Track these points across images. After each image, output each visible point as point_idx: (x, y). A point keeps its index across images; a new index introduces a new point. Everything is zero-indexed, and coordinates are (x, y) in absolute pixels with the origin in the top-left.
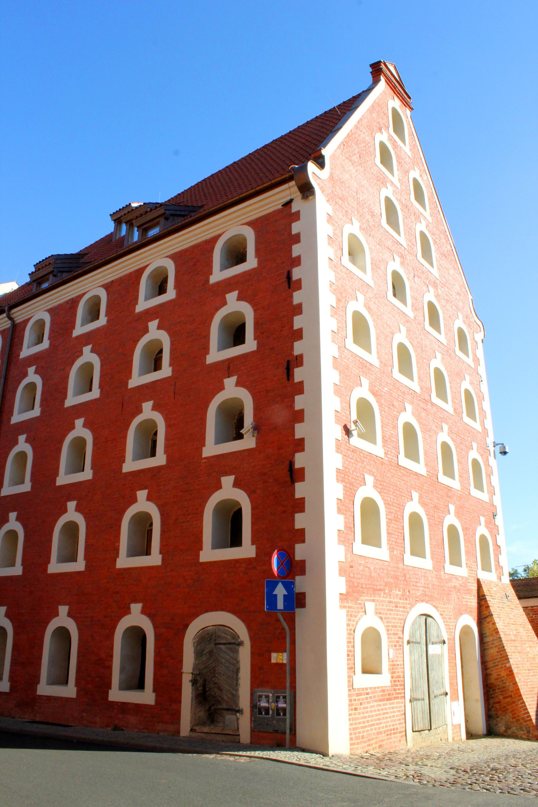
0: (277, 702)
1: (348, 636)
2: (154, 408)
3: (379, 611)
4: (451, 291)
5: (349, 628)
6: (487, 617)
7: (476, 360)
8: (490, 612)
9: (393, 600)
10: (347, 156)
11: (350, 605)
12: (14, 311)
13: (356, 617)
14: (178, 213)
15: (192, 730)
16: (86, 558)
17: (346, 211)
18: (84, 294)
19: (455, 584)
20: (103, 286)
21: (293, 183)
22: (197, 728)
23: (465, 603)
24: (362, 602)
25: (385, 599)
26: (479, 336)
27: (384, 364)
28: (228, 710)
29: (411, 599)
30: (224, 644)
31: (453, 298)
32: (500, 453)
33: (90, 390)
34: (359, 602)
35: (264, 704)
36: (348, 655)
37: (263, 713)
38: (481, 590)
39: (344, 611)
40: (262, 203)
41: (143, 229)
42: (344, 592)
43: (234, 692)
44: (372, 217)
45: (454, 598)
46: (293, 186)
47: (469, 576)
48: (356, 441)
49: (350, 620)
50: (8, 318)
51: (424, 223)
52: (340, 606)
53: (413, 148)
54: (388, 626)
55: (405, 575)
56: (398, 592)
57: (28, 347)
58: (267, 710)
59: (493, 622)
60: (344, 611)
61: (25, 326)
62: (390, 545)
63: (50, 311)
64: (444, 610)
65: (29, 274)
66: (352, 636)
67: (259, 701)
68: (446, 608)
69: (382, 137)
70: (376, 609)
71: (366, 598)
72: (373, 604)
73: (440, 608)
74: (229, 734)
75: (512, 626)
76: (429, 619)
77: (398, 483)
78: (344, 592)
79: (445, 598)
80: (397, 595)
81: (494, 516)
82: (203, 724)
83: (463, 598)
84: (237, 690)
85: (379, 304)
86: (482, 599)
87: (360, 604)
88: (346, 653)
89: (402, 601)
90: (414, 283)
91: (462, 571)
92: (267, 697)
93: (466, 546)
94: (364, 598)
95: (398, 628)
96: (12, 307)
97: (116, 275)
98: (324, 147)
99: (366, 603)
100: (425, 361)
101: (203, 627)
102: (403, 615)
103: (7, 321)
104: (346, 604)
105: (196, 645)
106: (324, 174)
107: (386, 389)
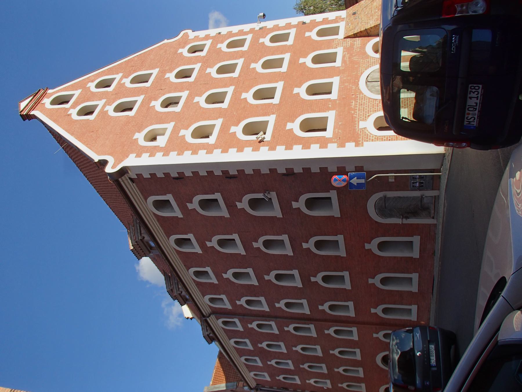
0: (416, 178)
1: (379, 140)
2: (256, 241)
3: (364, 118)
4: (165, 58)
5: (374, 140)
6: (367, 32)
7: (207, 37)
8: (364, 31)
9: (358, 107)
10: (94, 142)
11: (361, 139)
12: (252, 387)
13: (368, 135)
14: (139, 231)
15: (433, 218)
16: (342, 271)
17: (131, 143)
18: (193, 279)
19: (348, 58)
20: (188, 270)
21: (120, 179)
22: (432, 216)
23: (359, 49)
24: (360, 130)
25: (357, 113)
26: (191, 34)
27: (220, 114)
28: (421, 201)
29: (357, 94)
30: (385, 204)
31: (169, 56)
32: (264, 18)
33: (234, 240)
34: (359, 132)
35: (418, 184)
36: (389, 140)
37: (422, 185)
38: (351, 36)
39: (365, 143)
40: (157, 232)
41: (151, 250)
42: (354, 143)
43: (411, 199)
44: (130, 123)
45: (355, 58)
46: (122, 179)
47: (342, 46)
48: (268, 137)
49: (370, 139)
50: (209, 317)
51: (124, 80)
52: (362, 146)
53: (74, 88)
54: (373, 112)
55: (343, 98)
56: (353, 104)
57: (225, 305)
58: (420, 183)
59: (370, 28)
60: (365, 143)
61: (212, 307)
62: (326, 110)
63: (204, 296)
64: (363, 67)
65: (209, 344)
66: (379, 138)
67: (416, 187)
68: (362, 66)
69: (74, 113)
70: (363, 120)
71: (357, 128)
72: (360, 122)
73: (362, 70)
74: (435, 201)
75: (372, 12)
76: (369, 79)
77: (290, 103)
78: (354, 143)
79: (356, 66)
80: (355, 104)
81: (304, 23)
82: (430, 213)
83: (356, 51)
84: (410, 197)
85: (184, 118)
86: (356, 36)
87: (361, 132)
88: (388, 142)
89: (358, 101)
90: (166, 90)
91: (340, 51)
92: (413, 183)
93: (324, 49)
94: (357, 129)
95: (374, 103)
96: (204, 316)
97: (144, 204)
98: (93, 160)
99: (360, 128)
100: (213, 82)
101: (376, 214)
102: (367, 99)
103: (211, 318)
104: (361, 142)
105: (386, 218)
106: (111, 160)
107: (235, 113)
